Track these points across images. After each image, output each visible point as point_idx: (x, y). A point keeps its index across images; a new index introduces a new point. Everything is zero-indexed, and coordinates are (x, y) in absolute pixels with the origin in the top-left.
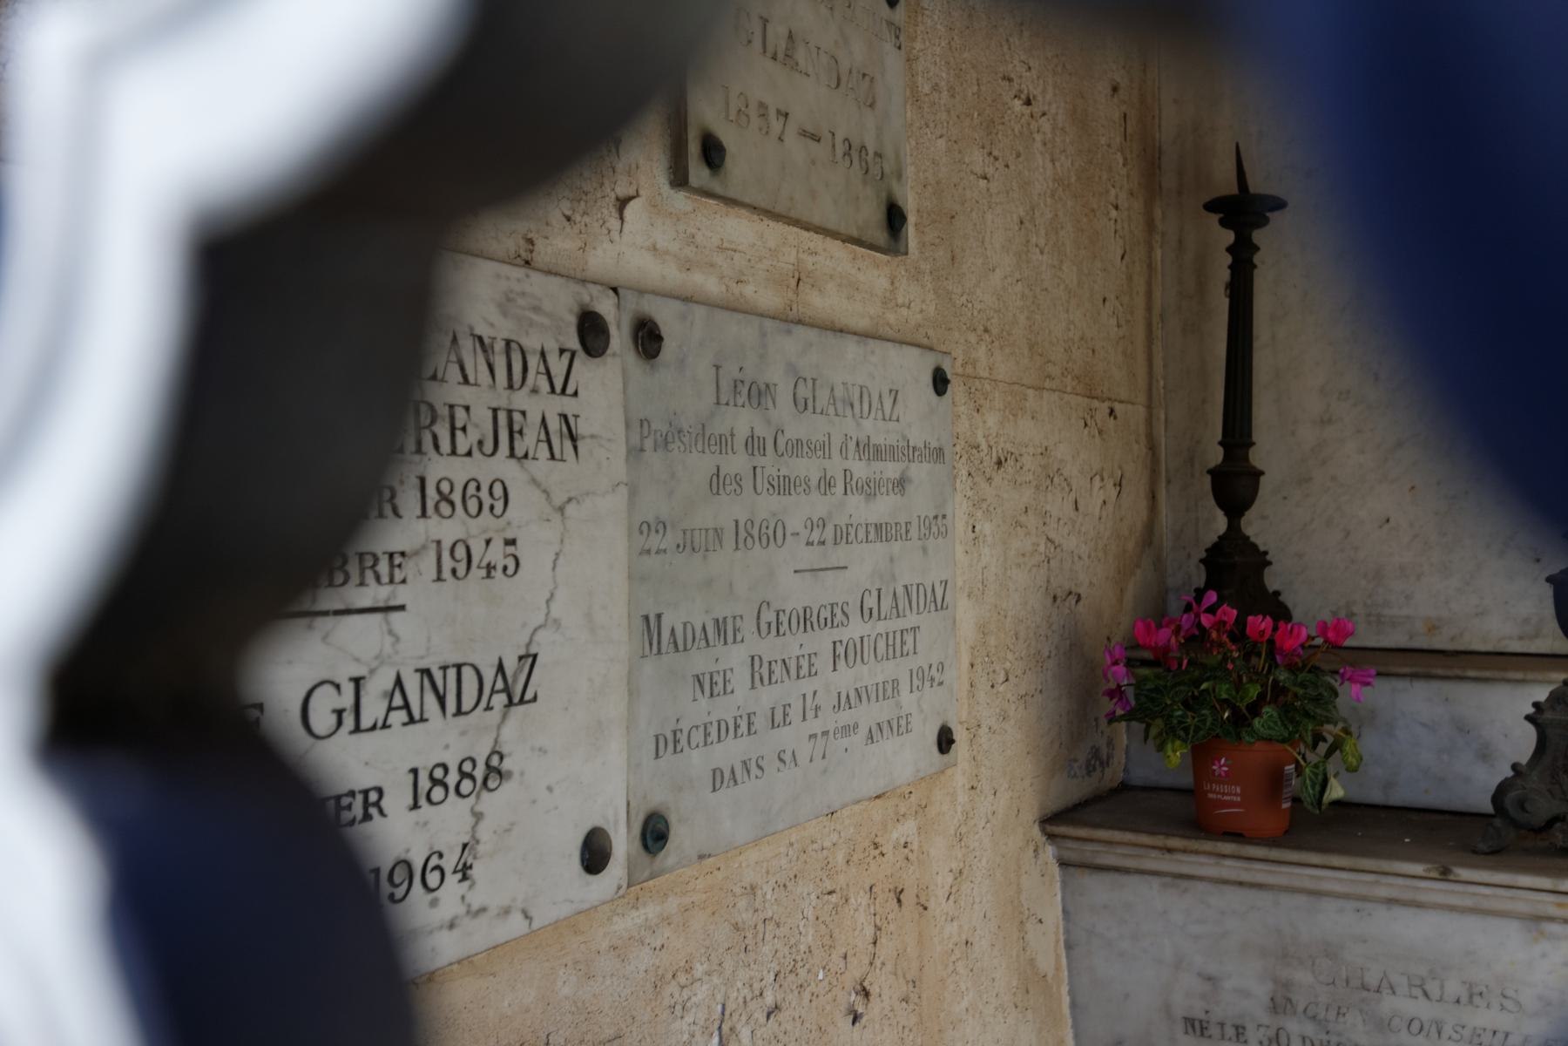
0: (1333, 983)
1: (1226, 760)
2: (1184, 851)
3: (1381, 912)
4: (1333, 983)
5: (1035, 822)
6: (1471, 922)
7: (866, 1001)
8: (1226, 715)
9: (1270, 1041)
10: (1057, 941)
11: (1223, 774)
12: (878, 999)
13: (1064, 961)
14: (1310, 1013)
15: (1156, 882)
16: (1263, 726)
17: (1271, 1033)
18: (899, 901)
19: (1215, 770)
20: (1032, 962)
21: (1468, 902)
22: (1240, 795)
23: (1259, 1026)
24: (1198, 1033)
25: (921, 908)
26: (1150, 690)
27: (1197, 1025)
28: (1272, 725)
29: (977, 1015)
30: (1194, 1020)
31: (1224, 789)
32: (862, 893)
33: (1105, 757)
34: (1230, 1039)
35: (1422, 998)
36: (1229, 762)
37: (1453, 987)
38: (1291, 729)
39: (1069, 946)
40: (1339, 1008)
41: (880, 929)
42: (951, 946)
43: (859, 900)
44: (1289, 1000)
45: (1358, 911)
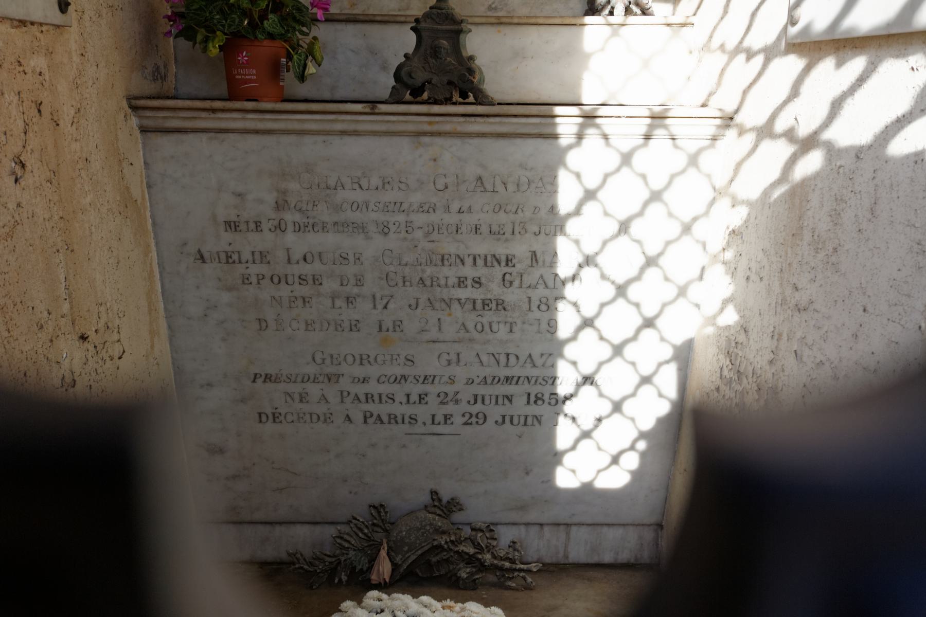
0: (311, 187)
1: (246, 53)
2: (223, 110)
3: (336, 140)
4: (311, 187)
5: (124, 97)
6: (385, 140)
7: (23, 170)
8: (246, 22)
9: (276, 228)
10: (142, 182)
11: (245, 62)
12: (31, 174)
13: (147, 196)
14: (298, 208)
15: (204, 136)
16: (269, 26)
17: (276, 223)
18: (39, 111)
19: (239, 60)
20: (128, 188)
21: (383, 127)
22: (256, 75)
23: (269, 219)
24: (233, 229)
25: (54, 124)
26: (196, 10)
27: (232, 224)
28: (274, 25)
29: (97, 211)
30: (230, 222)
31: (243, 72)
32: (12, 94)
33: (163, 74)
34: (252, 230)
35: (359, 190)
36: (249, 54)
37: (375, 181)
38: (286, 29)
39: (149, 186)
40: (314, 202)
41: (28, 125)
42: (76, 158)
43: (11, 98)
44: (286, 201)
45: (325, 142)
